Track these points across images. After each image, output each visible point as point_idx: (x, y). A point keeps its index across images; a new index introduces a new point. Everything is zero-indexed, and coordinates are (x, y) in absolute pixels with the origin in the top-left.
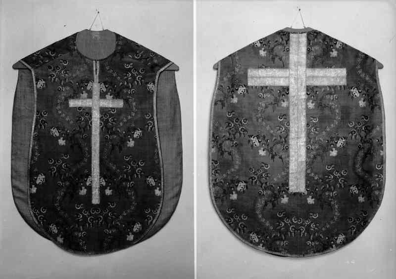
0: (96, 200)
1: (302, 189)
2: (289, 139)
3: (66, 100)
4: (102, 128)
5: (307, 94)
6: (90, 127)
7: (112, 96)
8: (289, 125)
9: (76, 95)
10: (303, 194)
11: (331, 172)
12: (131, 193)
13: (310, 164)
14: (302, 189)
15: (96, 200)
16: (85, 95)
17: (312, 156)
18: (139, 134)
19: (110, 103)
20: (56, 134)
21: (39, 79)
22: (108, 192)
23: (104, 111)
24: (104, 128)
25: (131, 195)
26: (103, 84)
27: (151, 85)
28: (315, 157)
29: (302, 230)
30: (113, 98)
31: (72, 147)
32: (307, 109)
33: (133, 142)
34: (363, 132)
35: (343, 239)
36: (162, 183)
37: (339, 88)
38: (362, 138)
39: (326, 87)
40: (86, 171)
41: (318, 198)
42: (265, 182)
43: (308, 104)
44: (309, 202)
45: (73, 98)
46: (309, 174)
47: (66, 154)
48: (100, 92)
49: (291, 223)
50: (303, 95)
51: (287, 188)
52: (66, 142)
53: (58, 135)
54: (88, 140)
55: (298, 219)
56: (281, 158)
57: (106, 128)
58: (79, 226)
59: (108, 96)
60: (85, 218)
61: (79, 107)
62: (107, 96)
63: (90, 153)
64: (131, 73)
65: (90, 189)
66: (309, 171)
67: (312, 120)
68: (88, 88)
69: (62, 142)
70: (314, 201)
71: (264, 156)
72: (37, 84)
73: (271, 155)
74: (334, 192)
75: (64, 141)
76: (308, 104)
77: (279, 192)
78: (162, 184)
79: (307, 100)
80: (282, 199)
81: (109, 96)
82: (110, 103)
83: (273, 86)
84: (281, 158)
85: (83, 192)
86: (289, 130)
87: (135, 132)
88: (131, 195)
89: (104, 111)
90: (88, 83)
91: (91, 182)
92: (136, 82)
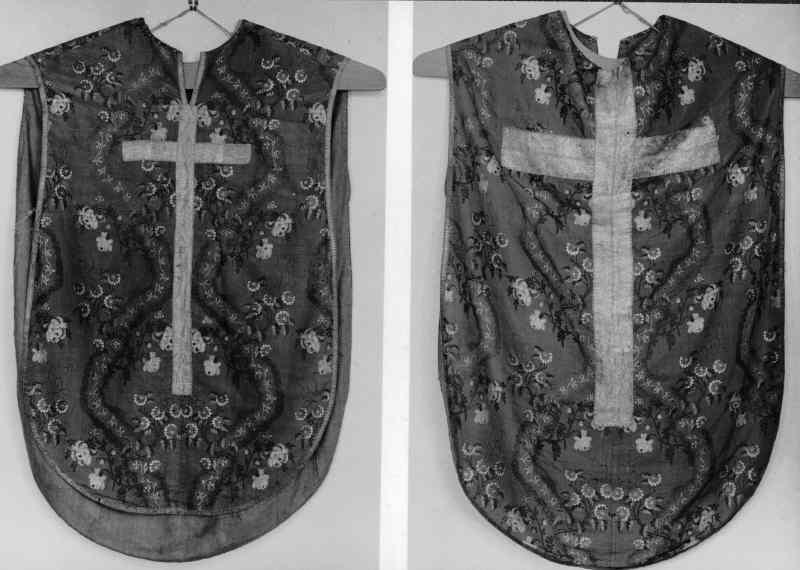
0: (182, 384)
1: (626, 420)
2: (591, 301)
3: (116, 143)
4: (200, 213)
5: (634, 197)
6: (172, 210)
7: (224, 137)
8: (592, 267)
9: (137, 130)
10: (625, 430)
11: (689, 372)
12: (262, 372)
13: (644, 358)
14: (626, 420)
15: (182, 384)
16: (161, 132)
17: (646, 338)
18: (286, 228)
19: (222, 153)
20: (90, 223)
21: (54, 93)
22: (212, 368)
23: (205, 172)
24: (204, 212)
25: (262, 378)
26: (205, 107)
27: (318, 111)
28: (653, 341)
29: (622, 514)
30: (227, 141)
31: (128, 256)
32: (635, 232)
33: (271, 246)
34: (756, 260)
35: (710, 520)
36: (335, 343)
37: (703, 173)
38: (754, 274)
39: (673, 174)
40: (159, 315)
41: (665, 435)
42: (540, 392)
43: (637, 220)
44: (639, 448)
45: (132, 139)
46: (641, 382)
47: (114, 270)
48: (198, 126)
49: (597, 498)
50: (626, 199)
51: (590, 414)
52: (113, 245)
53: (94, 224)
54: (167, 243)
55: (613, 489)
56: (576, 339)
57: (209, 212)
58: (141, 448)
59: (217, 137)
60: (157, 428)
61: (147, 161)
62: (211, 136)
63: (171, 272)
64: (275, 80)
65: (167, 358)
66: (640, 376)
67: (646, 255)
68: (170, 116)
69: (104, 244)
70: (653, 445)
71: (540, 332)
72: (50, 103)
73: (557, 330)
74: (699, 419)
75: (111, 241)
76: (637, 220)
77: (571, 422)
78: (336, 347)
79: (635, 212)
80: (576, 438)
81: (218, 136)
82: (222, 153)
83: (554, 178)
84: (576, 339)
85: (152, 364)
86: (592, 279)
87: (277, 224)
88: (262, 378)
89: (205, 172)
90: (169, 103)
91: (171, 341)
92: (283, 102)
